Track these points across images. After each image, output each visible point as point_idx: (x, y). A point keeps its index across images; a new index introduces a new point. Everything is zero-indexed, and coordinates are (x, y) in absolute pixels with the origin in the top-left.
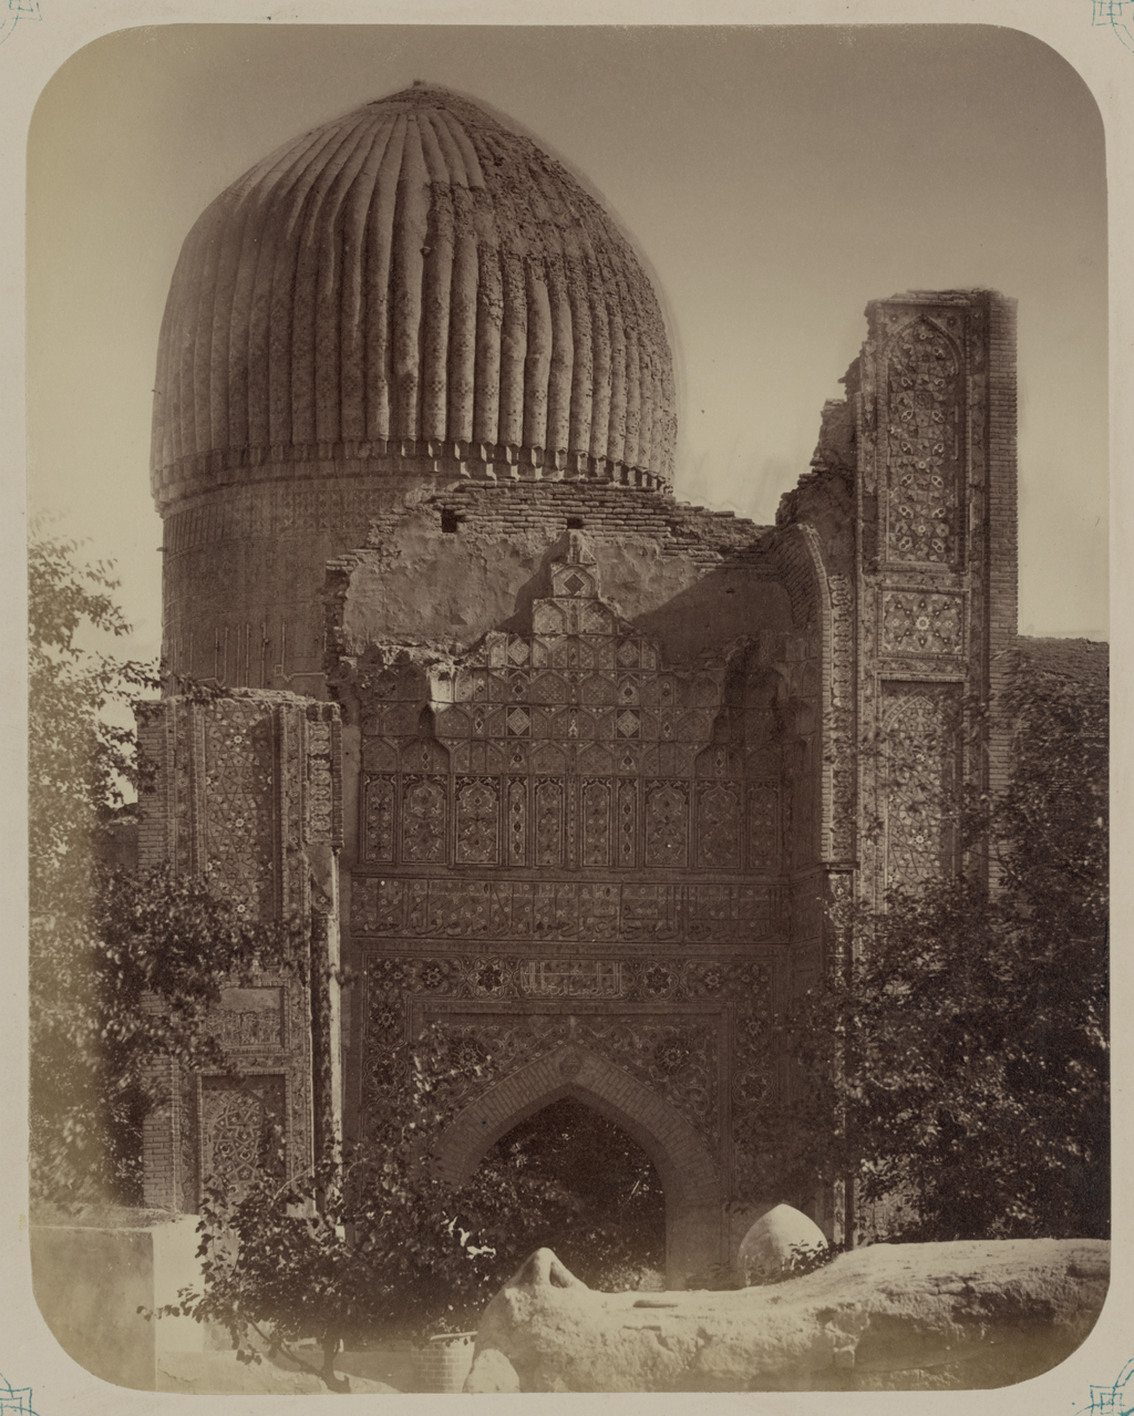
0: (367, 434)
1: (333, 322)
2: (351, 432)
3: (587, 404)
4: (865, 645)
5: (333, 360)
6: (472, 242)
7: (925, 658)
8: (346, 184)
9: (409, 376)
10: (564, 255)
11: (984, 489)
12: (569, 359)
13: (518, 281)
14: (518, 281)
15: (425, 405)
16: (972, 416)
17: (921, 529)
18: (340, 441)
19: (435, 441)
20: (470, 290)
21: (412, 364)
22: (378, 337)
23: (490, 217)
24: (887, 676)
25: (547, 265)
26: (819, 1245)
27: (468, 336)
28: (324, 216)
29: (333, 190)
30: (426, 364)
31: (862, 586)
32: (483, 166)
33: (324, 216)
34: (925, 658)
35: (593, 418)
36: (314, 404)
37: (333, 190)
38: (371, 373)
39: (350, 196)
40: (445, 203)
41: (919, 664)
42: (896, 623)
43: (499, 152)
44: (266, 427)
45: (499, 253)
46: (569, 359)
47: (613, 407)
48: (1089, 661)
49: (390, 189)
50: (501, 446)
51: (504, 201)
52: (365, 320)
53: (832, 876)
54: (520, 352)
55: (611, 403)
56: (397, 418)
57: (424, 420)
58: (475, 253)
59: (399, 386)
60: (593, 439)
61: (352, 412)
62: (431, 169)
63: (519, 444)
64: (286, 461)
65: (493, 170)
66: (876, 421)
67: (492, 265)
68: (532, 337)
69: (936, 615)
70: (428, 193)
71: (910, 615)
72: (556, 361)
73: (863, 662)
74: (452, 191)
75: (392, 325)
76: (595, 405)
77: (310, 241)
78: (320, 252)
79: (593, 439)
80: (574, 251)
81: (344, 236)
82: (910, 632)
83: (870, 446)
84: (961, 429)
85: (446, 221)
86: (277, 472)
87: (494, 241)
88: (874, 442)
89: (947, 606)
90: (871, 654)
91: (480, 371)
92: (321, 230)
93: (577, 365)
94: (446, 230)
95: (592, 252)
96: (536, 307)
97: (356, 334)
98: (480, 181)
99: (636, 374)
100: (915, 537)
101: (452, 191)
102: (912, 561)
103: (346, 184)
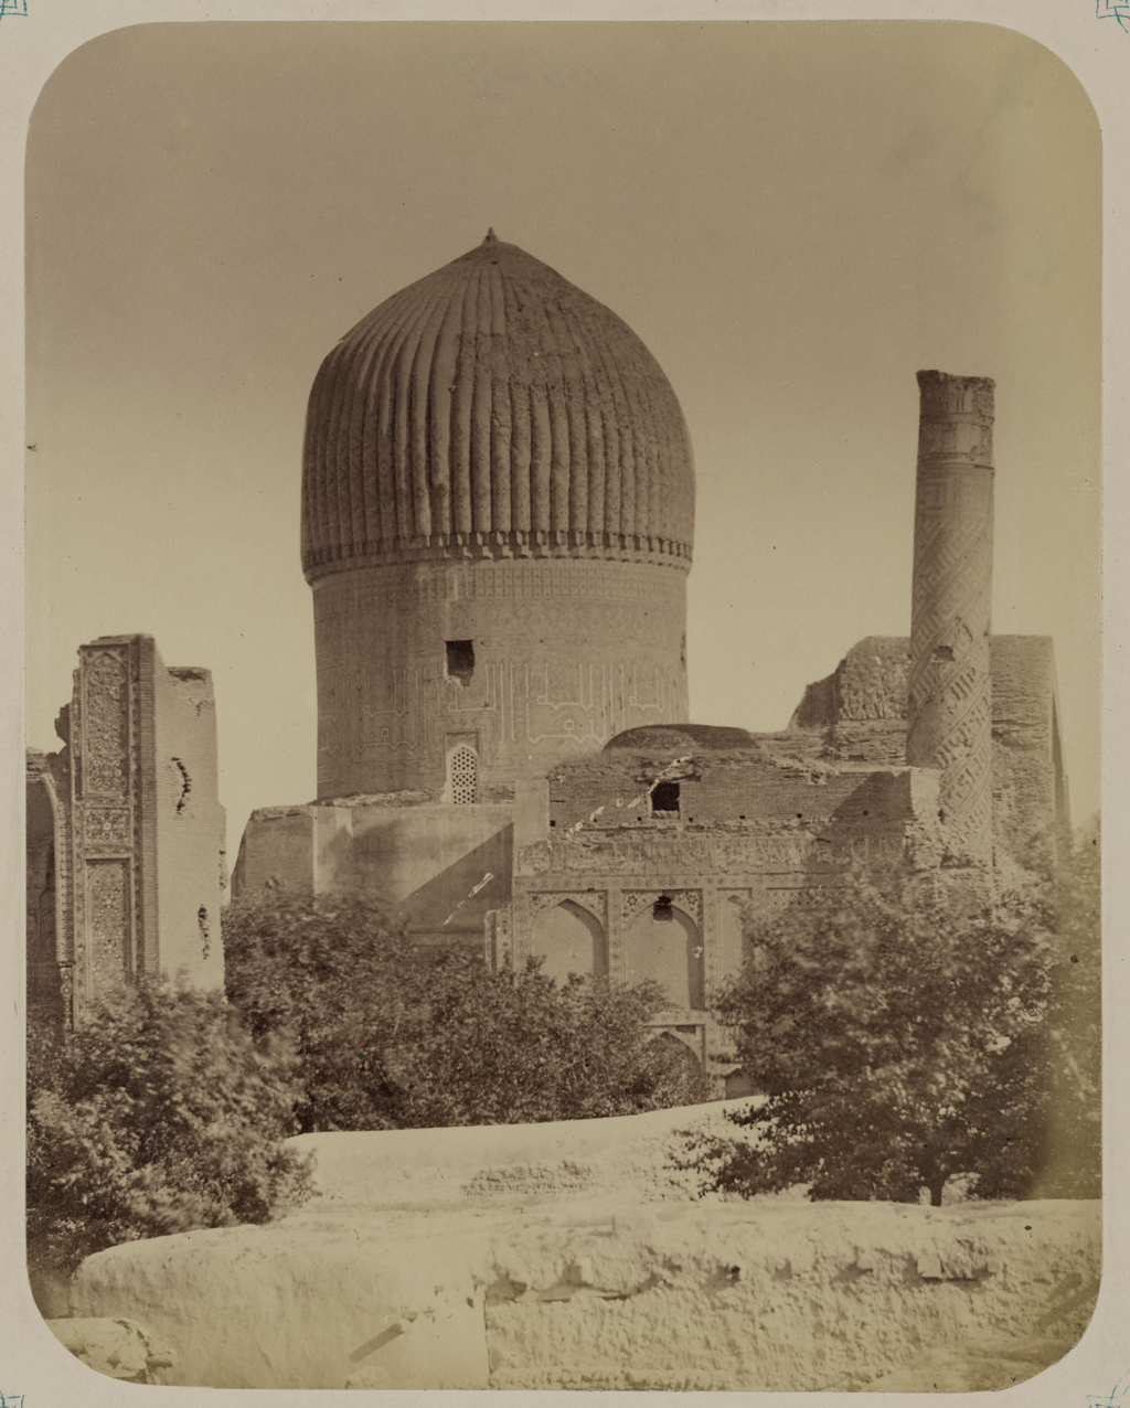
0: (415, 534)
1: (388, 449)
2: (405, 531)
3: (582, 492)
4: (76, 840)
5: (389, 479)
6: (486, 378)
7: (109, 846)
8: (401, 340)
9: (441, 487)
10: (564, 379)
11: (137, 748)
12: (565, 460)
13: (523, 405)
14: (523, 405)
15: (454, 506)
16: (132, 707)
17: (106, 773)
18: (397, 538)
19: (463, 533)
20: (484, 419)
21: (443, 477)
22: (418, 458)
23: (502, 357)
24: (88, 857)
25: (548, 389)
26: (314, 1183)
27: (482, 451)
28: (383, 370)
29: (392, 344)
30: (453, 477)
31: (73, 807)
32: (506, 314)
33: (383, 370)
34: (109, 846)
35: (589, 502)
36: (379, 510)
37: (392, 344)
38: (415, 485)
39: (402, 348)
40: (469, 351)
41: (107, 850)
42: (93, 827)
43: (524, 298)
44: (350, 530)
45: (509, 384)
46: (565, 460)
47: (607, 492)
48: (1036, 650)
49: (430, 341)
50: (513, 533)
51: (517, 342)
52: (410, 445)
53: (63, 970)
54: (524, 459)
55: (606, 488)
56: (436, 519)
57: (455, 519)
58: (488, 387)
59: (435, 493)
60: (590, 518)
61: (404, 516)
62: (464, 322)
63: (548, 530)
64: (379, 552)
65: (514, 313)
66: (80, 714)
67: (502, 394)
68: (534, 447)
69: (114, 822)
70: (458, 343)
71: (100, 823)
72: (554, 463)
73: (76, 850)
74: (476, 339)
75: (429, 448)
76: (590, 492)
77: (373, 390)
78: (380, 396)
79: (590, 518)
80: (572, 374)
81: (396, 383)
82: (101, 831)
83: (76, 729)
84: (125, 714)
85: (468, 362)
86: (390, 558)
87: (505, 377)
88: (79, 726)
89: (120, 816)
90: (80, 845)
91: (493, 476)
92: (381, 377)
93: (573, 463)
94: (468, 371)
95: (588, 373)
96: (536, 423)
97: (403, 458)
98: (500, 328)
99: (629, 462)
100: (103, 777)
101: (476, 339)
102: (102, 792)
103: (401, 340)
